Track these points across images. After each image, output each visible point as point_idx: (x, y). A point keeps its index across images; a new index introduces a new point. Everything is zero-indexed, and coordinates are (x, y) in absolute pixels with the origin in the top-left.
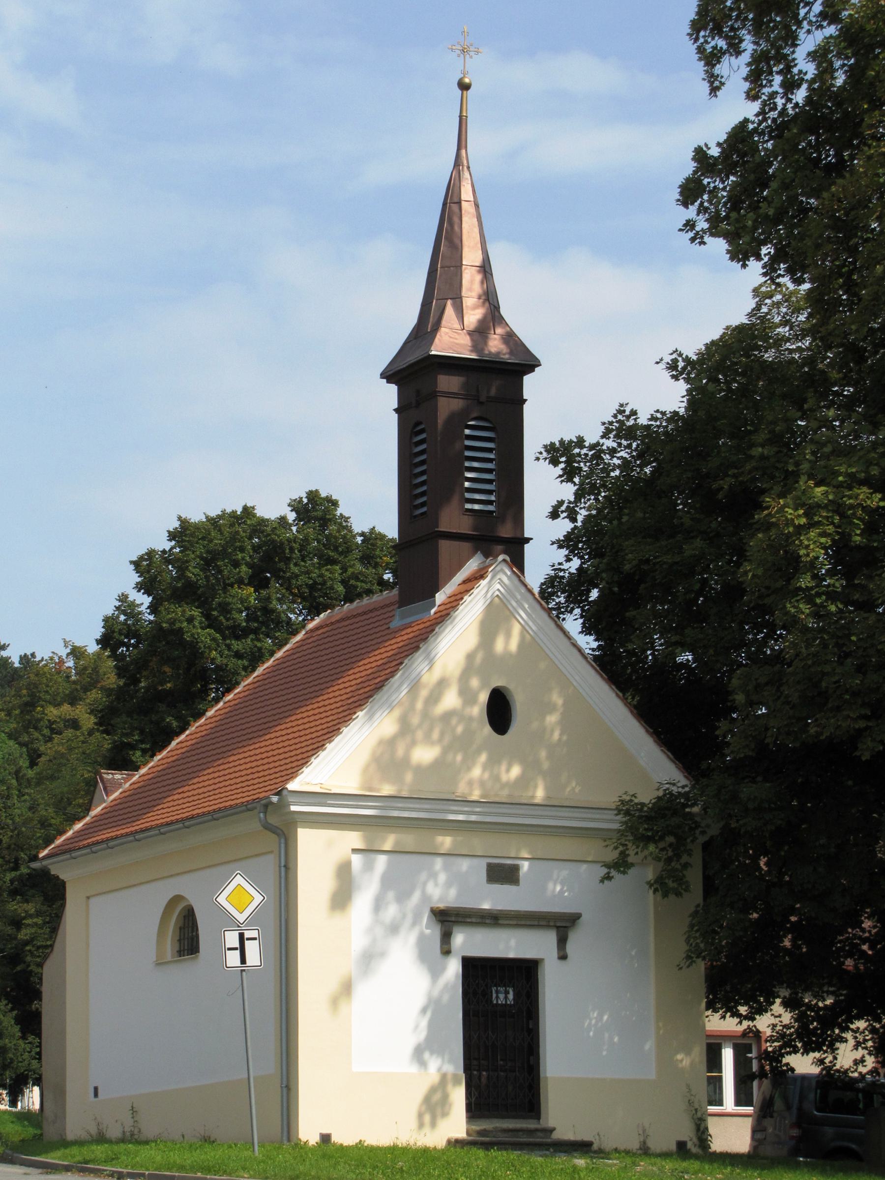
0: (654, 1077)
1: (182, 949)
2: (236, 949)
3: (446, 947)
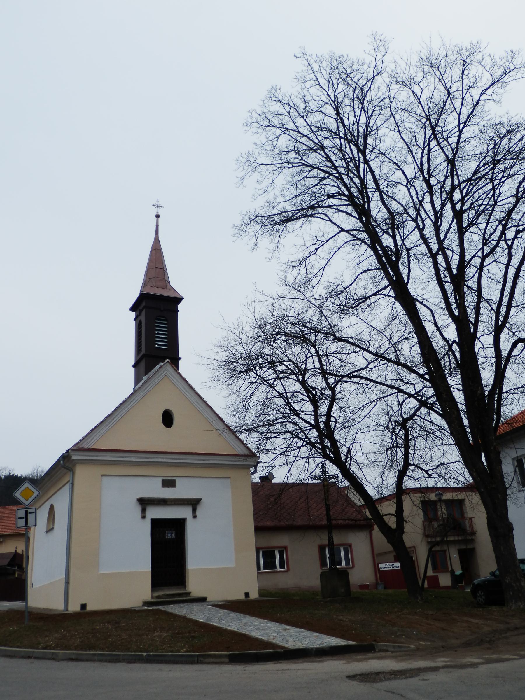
3: (143, 515)
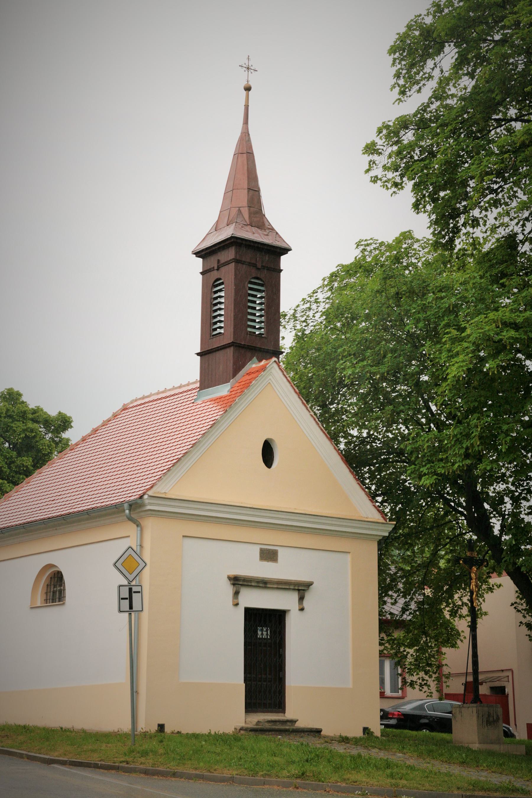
0: (350, 686)
1: (48, 598)
2: (127, 599)
3: (236, 601)
